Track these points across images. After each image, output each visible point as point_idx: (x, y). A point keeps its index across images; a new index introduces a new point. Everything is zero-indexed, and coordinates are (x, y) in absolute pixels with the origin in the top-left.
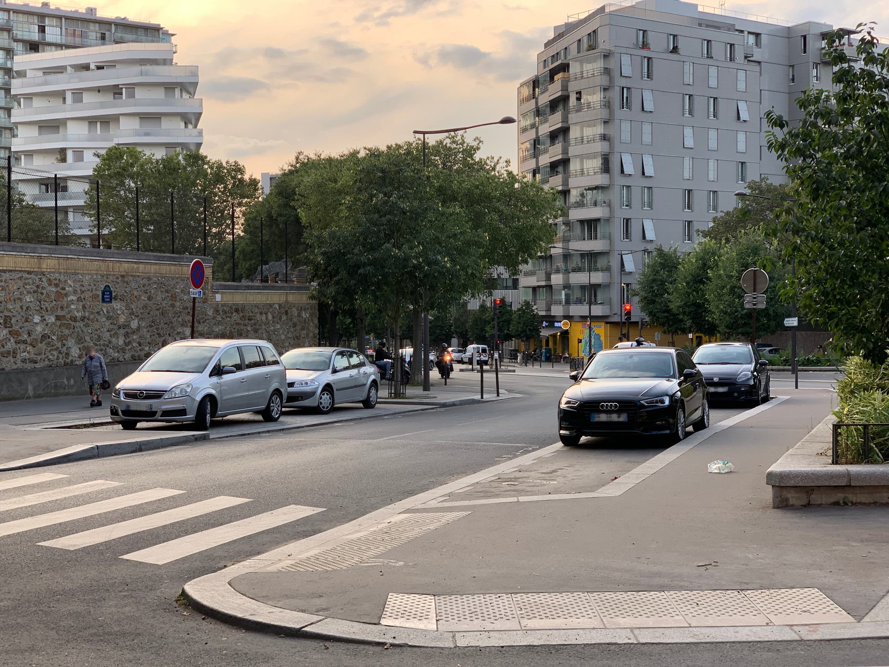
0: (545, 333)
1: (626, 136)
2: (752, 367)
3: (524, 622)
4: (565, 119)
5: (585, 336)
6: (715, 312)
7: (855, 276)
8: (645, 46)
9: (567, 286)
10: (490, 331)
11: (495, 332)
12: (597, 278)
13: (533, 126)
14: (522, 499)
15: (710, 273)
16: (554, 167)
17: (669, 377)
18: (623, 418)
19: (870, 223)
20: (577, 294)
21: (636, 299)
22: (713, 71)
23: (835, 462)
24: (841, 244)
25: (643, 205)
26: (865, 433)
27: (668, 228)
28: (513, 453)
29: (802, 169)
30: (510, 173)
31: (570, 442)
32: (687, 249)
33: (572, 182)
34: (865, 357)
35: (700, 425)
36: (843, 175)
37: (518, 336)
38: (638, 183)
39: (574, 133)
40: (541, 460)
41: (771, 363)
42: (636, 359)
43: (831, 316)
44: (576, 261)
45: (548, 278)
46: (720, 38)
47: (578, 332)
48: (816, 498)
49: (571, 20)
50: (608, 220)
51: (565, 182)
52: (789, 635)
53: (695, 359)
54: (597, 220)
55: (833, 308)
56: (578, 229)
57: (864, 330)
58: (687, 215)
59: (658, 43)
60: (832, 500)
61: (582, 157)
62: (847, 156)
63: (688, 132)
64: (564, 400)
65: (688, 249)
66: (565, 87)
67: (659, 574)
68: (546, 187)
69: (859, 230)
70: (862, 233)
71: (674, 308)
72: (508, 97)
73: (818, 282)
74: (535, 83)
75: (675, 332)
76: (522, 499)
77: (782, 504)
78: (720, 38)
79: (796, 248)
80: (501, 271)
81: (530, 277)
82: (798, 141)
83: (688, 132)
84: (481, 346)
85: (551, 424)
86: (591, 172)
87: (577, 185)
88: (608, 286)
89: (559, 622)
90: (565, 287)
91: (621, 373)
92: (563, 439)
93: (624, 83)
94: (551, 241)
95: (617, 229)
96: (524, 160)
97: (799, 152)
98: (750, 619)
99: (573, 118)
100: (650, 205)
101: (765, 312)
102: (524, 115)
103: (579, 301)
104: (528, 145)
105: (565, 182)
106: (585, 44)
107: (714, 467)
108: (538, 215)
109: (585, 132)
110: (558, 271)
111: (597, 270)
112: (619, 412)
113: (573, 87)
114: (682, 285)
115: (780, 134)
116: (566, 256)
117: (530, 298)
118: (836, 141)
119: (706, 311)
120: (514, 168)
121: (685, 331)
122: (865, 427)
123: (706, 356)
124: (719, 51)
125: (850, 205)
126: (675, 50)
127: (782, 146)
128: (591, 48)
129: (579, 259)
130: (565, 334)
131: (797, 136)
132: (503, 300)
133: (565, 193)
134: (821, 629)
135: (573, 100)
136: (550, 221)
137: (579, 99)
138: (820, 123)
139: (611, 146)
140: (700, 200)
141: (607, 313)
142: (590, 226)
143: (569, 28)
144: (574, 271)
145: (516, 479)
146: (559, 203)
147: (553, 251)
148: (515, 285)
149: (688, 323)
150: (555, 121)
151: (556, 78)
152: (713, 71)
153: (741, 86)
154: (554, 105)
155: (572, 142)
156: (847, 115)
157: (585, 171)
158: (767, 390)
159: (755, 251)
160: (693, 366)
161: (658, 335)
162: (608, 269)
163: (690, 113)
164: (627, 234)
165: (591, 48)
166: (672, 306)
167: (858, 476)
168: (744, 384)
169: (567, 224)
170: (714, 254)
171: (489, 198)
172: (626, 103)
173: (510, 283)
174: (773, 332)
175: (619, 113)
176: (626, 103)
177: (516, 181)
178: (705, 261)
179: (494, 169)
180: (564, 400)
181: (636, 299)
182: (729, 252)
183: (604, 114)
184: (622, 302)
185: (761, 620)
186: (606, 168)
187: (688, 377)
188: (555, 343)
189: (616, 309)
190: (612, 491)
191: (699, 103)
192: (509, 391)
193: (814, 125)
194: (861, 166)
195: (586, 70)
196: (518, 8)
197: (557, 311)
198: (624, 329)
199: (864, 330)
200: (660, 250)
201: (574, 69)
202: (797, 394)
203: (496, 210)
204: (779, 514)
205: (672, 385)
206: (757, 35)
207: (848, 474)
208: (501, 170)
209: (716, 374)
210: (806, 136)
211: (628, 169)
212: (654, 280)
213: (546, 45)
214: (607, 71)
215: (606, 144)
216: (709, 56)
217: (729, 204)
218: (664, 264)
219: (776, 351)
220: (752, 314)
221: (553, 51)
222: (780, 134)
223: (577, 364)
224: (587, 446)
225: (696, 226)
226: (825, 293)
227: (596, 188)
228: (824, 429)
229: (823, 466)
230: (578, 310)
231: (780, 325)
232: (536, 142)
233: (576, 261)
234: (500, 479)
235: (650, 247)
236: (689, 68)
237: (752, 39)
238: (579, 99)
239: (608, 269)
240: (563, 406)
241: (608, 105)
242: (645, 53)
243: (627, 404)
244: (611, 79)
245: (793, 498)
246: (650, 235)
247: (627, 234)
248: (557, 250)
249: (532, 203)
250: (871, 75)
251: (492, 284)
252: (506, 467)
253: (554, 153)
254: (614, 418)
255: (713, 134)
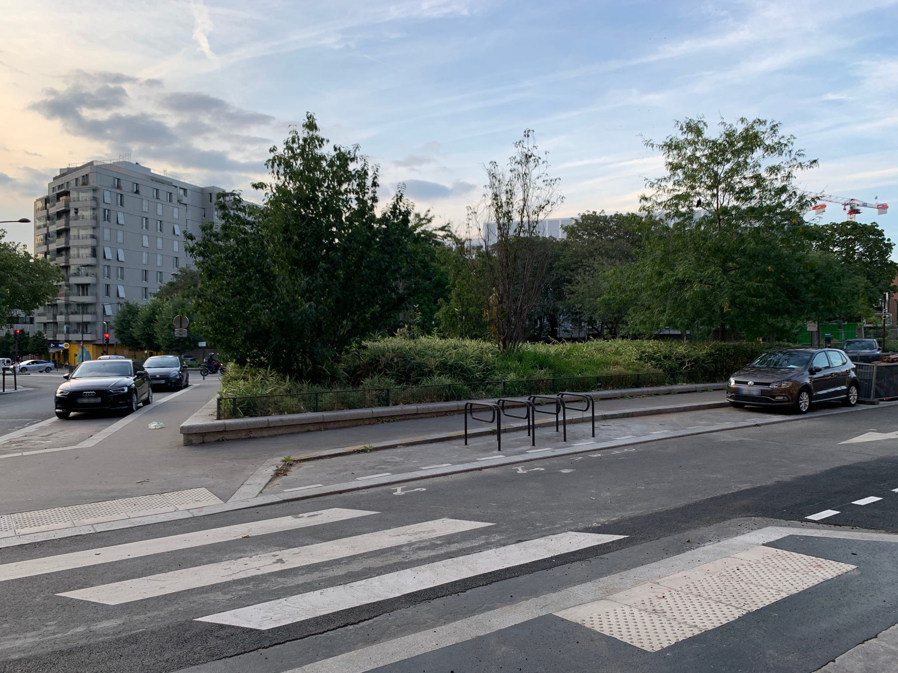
0: (51, 351)
1: (107, 236)
2: (178, 369)
3: (18, 531)
4: (67, 223)
5: (79, 353)
6: (160, 340)
7: (230, 321)
8: (119, 187)
9: (67, 323)
10: (13, 349)
11: (16, 350)
12: (87, 318)
13: (45, 226)
14: (25, 454)
15: (157, 317)
16: (59, 251)
17: (128, 376)
18: (99, 400)
19: (239, 294)
20: (75, 327)
21: (112, 331)
22: (160, 206)
23: (219, 419)
24: (224, 303)
25: (117, 277)
26: (234, 402)
27: (133, 291)
28: (22, 425)
29: (203, 263)
30: (26, 253)
31: (63, 416)
32: (144, 303)
33: (71, 261)
34: (236, 363)
35: (147, 402)
36: (225, 268)
37: (33, 353)
38: (114, 265)
39: (73, 232)
40: (42, 429)
41: (190, 366)
42: (107, 365)
43: (219, 341)
44: (74, 308)
45: (55, 318)
46: (163, 188)
47: (75, 350)
48: (207, 439)
49: (71, 166)
50: (95, 285)
51: (67, 261)
52: (187, 515)
53: (145, 365)
54: (88, 285)
55: (219, 337)
56: (75, 289)
57: (236, 349)
58: (145, 284)
59: (127, 187)
60: (217, 439)
61: (78, 247)
62: (227, 258)
63: (145, 238)
64: (59, 391)
65: (144, 303)
66: (67, 205)
67: (112, 491)
68: (52, 263)
69: (233, 296)
70: (235, 299)
71: (135, 335)
72: (28, 207)
73: (212, 323)
74: (47, 200)
75: (136, 350)
76: (25, 454)
77: (188, 443)
78: (163, 188)
79: (199, 305)
80: (19, 313)
81: (41, 316)
82: (204, 248)
83: (145, 238)
84: (6, 359)
85: (50, 405)
86: (85, 256)
87: (74, 263)
88: (95, 323)
89: (44, 528)
90: (66, 323)
91: (98, 374)
92: (58, 414)
93: (106, 207)
94: (55, 295)
95: (101, 290)
96: (38, 246)
97: (201, 254)
98: (166, 509)
99: (72, 223)
100: (122, 277)
101: (187, 339)
102: (39, 219)
103: (76, 332)
104: (42, 237)
105: (67, 261)
106: (80, 182)
107: (152, 426)
108: (45, 279)
109: (80, 234)
110: (61, 314)
111: (88, 313)
112: (96, 396)
113: (72, 205)
114: (140, 323)
115: (191, 243)
116: (67, 305)
117: (42, 329)
118: (221, 249)
119: (155, 338)
120: (31, 251)
121: (142, 349)
122: (234, 399)
123: (152, 363)
124: (162, 195)
125: (228, 284)
126: (137, 192)
127: (192, 250)
128: (84, 184)
129: (76, 307)
130: (66, 352)
131: (200, 245)
132: (22, 331)
133: (67, 267)
134: (205, 509)
135: (72, 213)
136: (55, 284)
137: (76, 213)
138: (213, 239)
139: (98, 242)
140: (152, 276)
141: (94, 339)
142: (84, 287)
143: (70, 171)
144: (72, 313)
145: (22, 441)
146: (63, 272)
147: (58, 302)
148: (32, 321)
149: (144, 345)
150: (60, 224)
151: (61, 198)
152: (160, 206)
153: (176, 216)
154: (59, 215)
155: (72, 238)
156: (227, 237)
157: (80, 256)
158: (187, 381)
159: (183, 306)
160: (143, 369)
161: (126, 352)
162: (95, 313)
163: (146, 227)
164: (108, 294)
165: (84, 184)
166: (134, 335)
167: (230, 425)
168: (174, 378)
169: (68, 286)
170: (159, 306)
171: (11, 267)
172: (107, 218)
173: (28, 320)
174: (192, 350)
175: (103, 224)
176: (107, 218)
177: (31, 258)
178: (154, 310)
179: (15, 250)
180: (59, 391)
181: (112, 331)
182: (168, 306)
183: (93, 223)
184: (104, 333)
185: (172, 509)
186: (94, 254)
187: (139, 375)
188: (59, 357)
189: (100, 336)
190: (88, 444)
191: (152, 223)
192: (24, 387)
193: (209, 240)
194: (234, 264)
195: (81, 198)
196: (35, 154)
197: (60, 337)
198: (105, 348)
199: (236, 349)
200: (128, 304)
201: (73, 195)
202: (204, 383)
203: (16, 275)
204: (186, 448)
205: (130, 380)
206: (185, 190)
207: (225, 424)
208: (20, 250)
209: (158, 373)
210: (205, 246)
211: (108, 256)
212: (124, 320)
213: (54, 179)
214: (95, 199)
215: (94, 241)
216: (158, 198)
217: (168, 279)
218: (131, 311)
219: (194, 360)
220: (181, 341)
221: (59, 182)
222: (191, 243)
223: (72, 369)
224: (74, 418)
225: (150, 290)
226: (215, 329)
227: (88, 266)
228: (214, 402)
229: (212, 421)
230: (78, 337)
231: (196, 346)
232: (47, 236)
233: (74, 308)
234: (10, 442)
235: (122, 301)
236: (145, 203)
237: (182, 192)
238: (76, 213)
239: (95, 313)
240: (58, 395)
241: (95, 218)
242: (119, 191)
243: (101, 392)
244: (98, 204)
245: (195, 439)
246: (122, 294)
247: (108, 294)
248: (61, 301)
249: (42, 272)
250: (239, 217)
251: (14, 320)
252: (17, 434)
253: (60, 243)
254: (92, 400)
255: (159, 240)
